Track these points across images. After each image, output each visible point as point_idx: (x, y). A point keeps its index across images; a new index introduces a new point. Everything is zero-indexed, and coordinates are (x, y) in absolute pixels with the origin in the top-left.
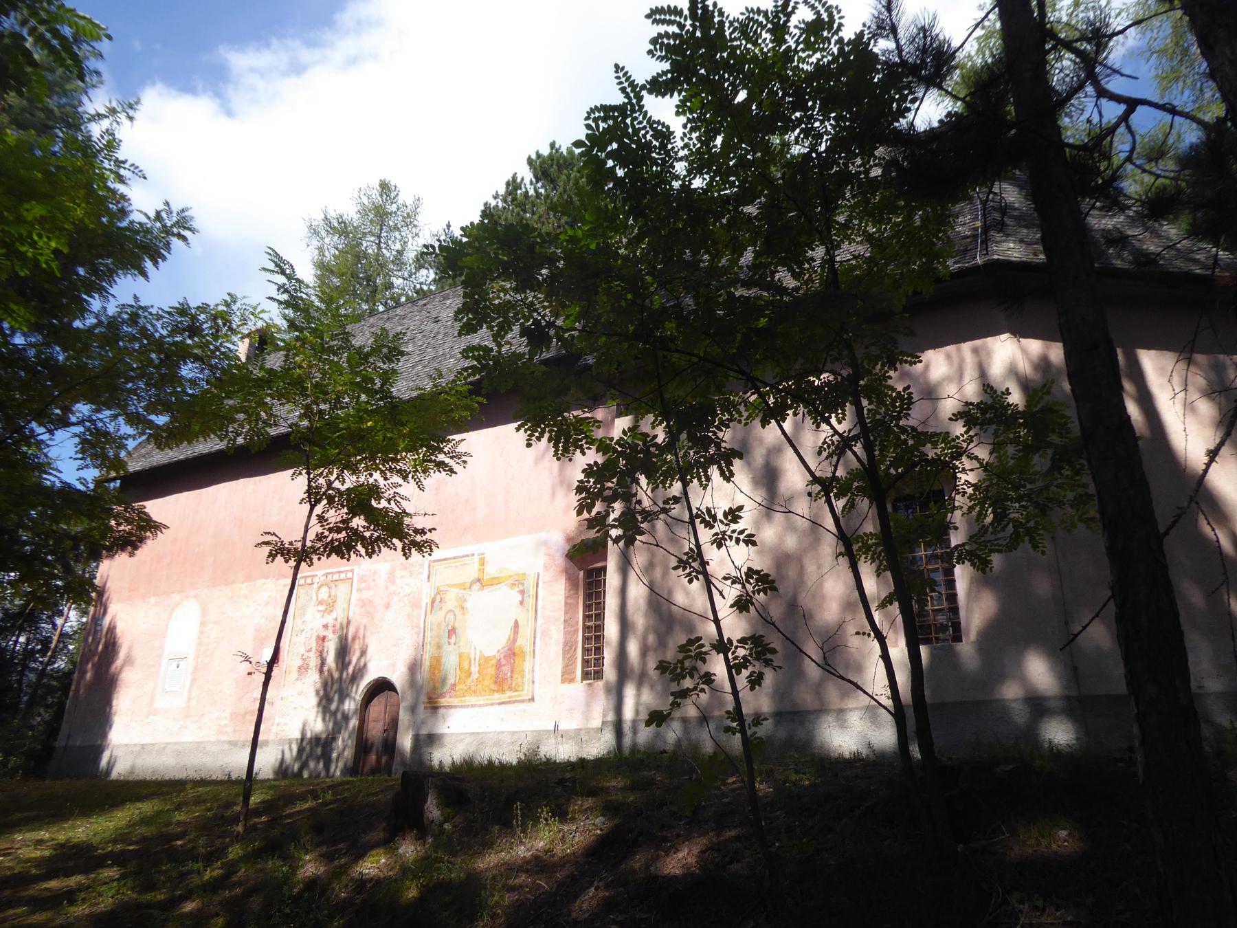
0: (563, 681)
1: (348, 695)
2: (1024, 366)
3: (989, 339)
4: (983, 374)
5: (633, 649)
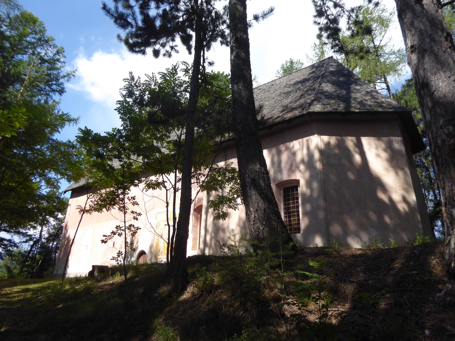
0: (192, 250)
1: (133, 256)
2: (322, 146)
3: (312, 137)
4: (308, 149)
5: (208, 238)
